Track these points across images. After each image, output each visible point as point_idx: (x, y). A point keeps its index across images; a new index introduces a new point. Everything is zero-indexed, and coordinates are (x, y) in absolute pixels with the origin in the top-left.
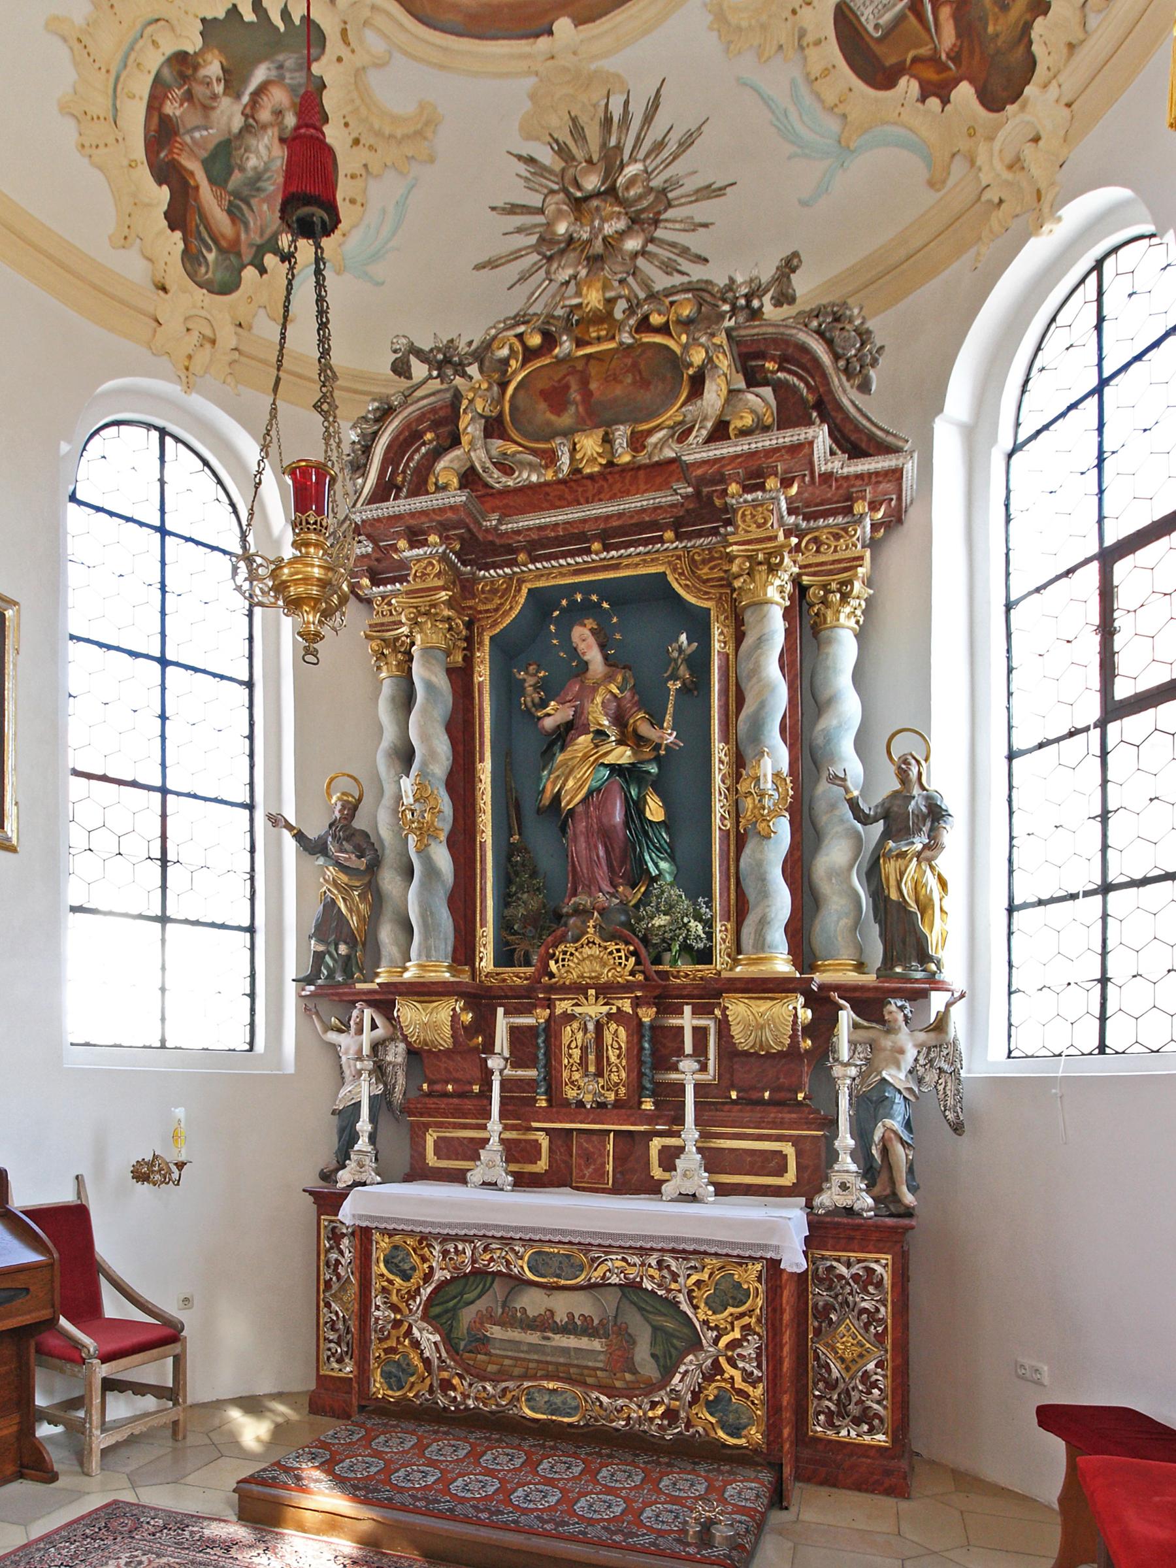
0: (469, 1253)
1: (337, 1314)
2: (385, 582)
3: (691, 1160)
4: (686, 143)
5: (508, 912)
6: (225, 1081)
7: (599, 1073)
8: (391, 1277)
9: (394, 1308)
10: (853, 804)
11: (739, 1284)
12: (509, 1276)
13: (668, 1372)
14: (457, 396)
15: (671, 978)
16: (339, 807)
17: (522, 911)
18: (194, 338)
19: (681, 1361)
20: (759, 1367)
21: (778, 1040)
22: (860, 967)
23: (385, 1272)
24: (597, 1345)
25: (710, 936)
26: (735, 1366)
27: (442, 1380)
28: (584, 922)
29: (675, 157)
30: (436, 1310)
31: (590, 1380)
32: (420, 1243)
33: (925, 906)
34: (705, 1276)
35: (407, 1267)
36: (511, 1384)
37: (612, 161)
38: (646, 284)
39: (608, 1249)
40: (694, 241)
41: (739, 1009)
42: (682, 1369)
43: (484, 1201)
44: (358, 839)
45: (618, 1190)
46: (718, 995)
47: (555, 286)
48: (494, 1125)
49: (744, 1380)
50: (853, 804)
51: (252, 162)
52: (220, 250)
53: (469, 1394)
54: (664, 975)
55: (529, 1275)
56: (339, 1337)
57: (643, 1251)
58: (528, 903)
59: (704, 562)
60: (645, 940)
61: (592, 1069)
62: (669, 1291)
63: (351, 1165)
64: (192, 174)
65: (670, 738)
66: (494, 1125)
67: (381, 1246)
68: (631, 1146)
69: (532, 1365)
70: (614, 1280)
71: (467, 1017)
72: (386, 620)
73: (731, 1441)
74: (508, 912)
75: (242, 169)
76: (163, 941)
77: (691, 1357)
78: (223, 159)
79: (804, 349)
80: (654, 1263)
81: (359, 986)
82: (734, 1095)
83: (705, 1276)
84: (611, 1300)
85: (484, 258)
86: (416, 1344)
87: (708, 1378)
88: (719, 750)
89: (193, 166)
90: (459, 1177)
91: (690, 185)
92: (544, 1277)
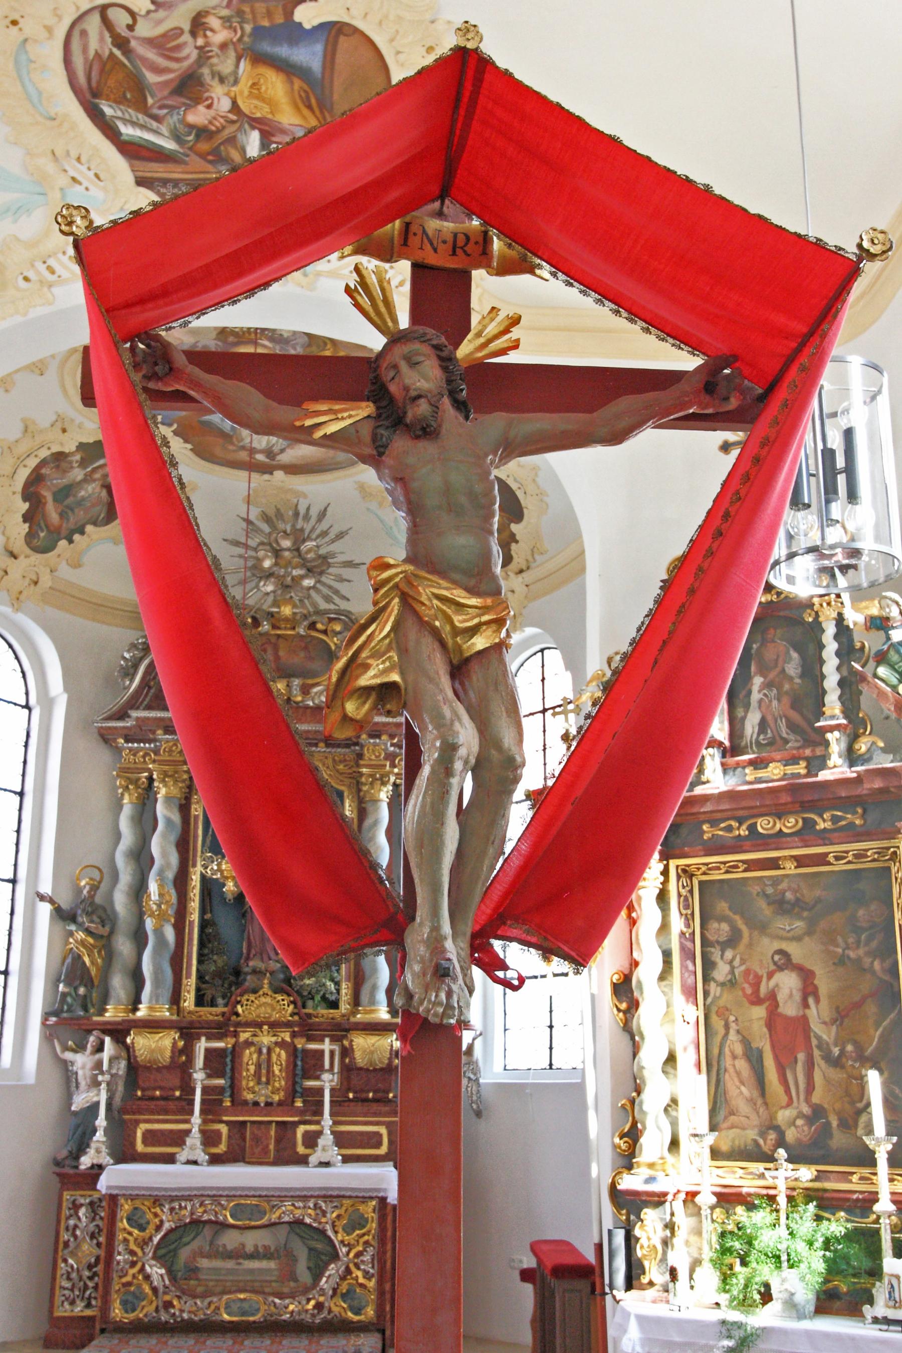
0: (189, 1208)
1: (72, 1267)
2: (133, 742)
3: (327, 1139)
4: (340, 536)
5: (203, 967)
7: (268, 1083)
8: (131, 1229)
9: (132, 1253)
11: (363, 1215)
12: (216, 1223)
13: (317, 1277)
16: (87, 888)
17: (213, 968)
18: (27, 581)
19: (326, 1268)
20: (373, 1267)
21: (381, 1059)
23: (127, 1226)
24: (272, 1264)
25: (338, 991)
26: (359, 1268)
27: (165, 1302)
28: (262, 981)
29: (333, 541)
30: (162, 1252)
31: (267, 1290)
32: (154, 1203)
34: (342, 1211)
35: (143, 1221)
36: (215, 1299)
37: (299, 537)
38: (315, 605)
39: (282, 1198)
41: (361, 1043)
42: (327, 1274)
43: (191, 1172)
44: (100, 912)
45: (276, 1162)
46: (347, 1030)
47: (260, 594)
48: (196, 1119)
49: (364, 1277)
52: (49, 531)
53: (185, 1309)
54: (309, 1016)
55: (231, 1221)
56: (73, 1285)
58: (219, 961)
59: (340, 762)
60: (298, 992)
61: (264, 1079)
62: (320, 1223)
63: (91, 1151)
64: (45, 497)
66: (196, 1119)
67: (126, 1207)
69: (228, 1284)
70: (286, 1219)
71: (181, 1044)
72: (132, 766)
73: (356, 1318)
74: (203, 967)
75: (75, 496)
77: (333, 1266)
78: (64, 493)
80: (311, 1205)
81: (96, 1019)
82: (351, 1095)
83: (342, 1211)
84: (283, 1231)
86: (147, 1277)
87: (343, 1278)
90: (170, 1159)
91: (341, 558)
92: (239, 1220)
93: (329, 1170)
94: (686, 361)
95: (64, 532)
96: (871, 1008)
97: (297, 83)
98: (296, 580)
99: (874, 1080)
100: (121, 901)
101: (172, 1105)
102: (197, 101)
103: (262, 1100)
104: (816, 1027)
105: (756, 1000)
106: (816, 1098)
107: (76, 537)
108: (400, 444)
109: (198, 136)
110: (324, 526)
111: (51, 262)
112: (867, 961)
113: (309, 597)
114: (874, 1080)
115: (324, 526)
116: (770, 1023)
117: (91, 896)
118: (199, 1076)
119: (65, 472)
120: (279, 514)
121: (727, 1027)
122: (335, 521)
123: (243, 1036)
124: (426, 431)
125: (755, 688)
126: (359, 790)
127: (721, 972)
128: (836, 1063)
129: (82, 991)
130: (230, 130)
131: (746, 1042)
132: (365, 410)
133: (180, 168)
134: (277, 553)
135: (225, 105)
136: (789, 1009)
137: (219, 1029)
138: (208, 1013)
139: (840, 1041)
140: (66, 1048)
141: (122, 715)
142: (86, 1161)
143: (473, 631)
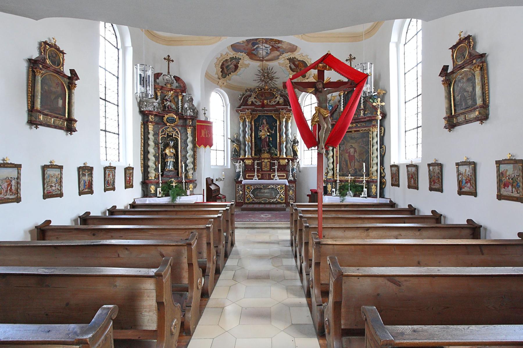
4: (275, 73)
6: (225, 170)
15: (273, 157)
40: (276, 82)
41: (281, 161)
43: (256, 180)
48: (256, 173)
66: (256, 173)
68: (270, 175)
76: (106, 136)
93: (277, 180)
99: (364, 164)
100: (241, 139)
104: (356, 157)
105: (347, 153)
108: (318, 93)
114: (364, 164)
116: (349, 156)
118: (256, 167)
120: (265, 69)
124: (321, 92)
127: (342, 148)
128: (359, 162)
131: (345, 159)
132: (314, 89)
134: (264, 76)
137: (259, 159)
138: (257, 157)
139: (360, 159)
141: (240, 107)
142: (239, 180)
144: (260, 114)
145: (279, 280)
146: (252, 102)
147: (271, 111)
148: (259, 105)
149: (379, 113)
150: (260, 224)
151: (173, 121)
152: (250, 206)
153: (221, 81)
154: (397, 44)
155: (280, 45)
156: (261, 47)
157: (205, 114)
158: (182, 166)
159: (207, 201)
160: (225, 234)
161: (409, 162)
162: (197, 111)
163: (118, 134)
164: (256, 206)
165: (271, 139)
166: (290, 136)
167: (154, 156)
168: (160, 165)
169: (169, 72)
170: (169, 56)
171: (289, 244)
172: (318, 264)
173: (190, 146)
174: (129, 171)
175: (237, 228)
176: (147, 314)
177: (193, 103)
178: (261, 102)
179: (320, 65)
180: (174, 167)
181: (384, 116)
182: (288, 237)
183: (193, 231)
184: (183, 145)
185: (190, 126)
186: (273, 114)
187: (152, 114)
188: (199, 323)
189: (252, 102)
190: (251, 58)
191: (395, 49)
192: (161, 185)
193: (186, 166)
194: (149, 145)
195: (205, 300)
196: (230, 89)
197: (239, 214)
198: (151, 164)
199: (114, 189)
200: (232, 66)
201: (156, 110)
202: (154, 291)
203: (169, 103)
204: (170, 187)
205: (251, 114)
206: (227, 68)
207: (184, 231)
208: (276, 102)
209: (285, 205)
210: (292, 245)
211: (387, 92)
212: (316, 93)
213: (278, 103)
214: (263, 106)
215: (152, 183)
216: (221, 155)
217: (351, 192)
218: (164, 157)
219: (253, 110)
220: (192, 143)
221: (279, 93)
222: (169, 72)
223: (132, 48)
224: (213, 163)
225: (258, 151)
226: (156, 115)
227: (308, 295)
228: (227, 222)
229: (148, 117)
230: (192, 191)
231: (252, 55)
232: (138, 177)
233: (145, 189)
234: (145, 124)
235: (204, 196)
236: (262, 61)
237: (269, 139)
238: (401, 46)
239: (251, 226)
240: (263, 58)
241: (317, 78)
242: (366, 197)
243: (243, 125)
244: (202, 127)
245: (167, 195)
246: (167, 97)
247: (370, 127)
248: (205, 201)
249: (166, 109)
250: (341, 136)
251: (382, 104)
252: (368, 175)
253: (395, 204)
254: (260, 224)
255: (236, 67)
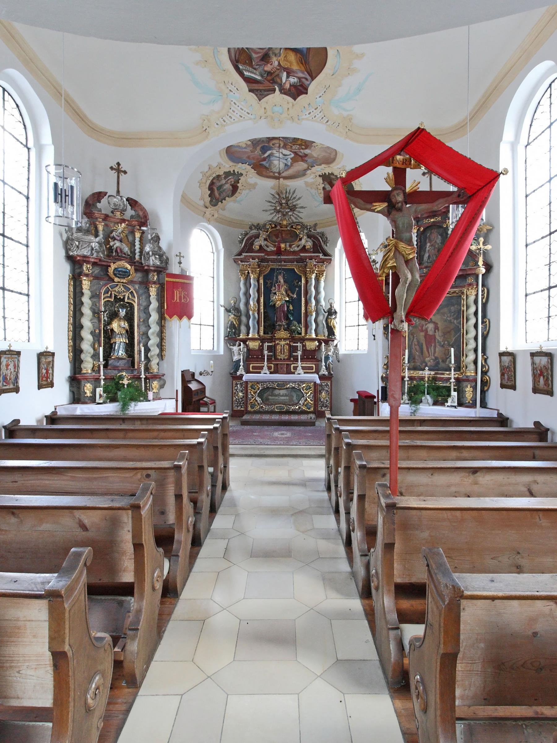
4: (299, 199)
6: (215, 357)
10: (324, 310)
14: (259, 234)
15: (295, 338)
22: (324, 336)
29: (297, 200)
33: (334, 327)
38: (292, 220)
40: (300, 214)
43: (265, 375)
48: (266, 363)
50: (324, 310)
51: (225, 187)
53: (266, 408)
57: (295, 382)
65: (295, 296)
66: (266, 363)
68: (288, 366)
76: (4, 298)
79: (317, 238)
85: (264, 209)
86: (256, 401)
87: (305, 401)
88: (303, 299)
89: (215, 188)
90: (260, 373)
93: (300, 375)
94: (452, 188)
95: (220, 200)
96: (453, 333)
97: (299, 55)
98: (287, 213)
99: (452, 350)
100: (242, 307)
101: (259, 359)
102: (268, 62)
103: (282, 358)
104: (437, 337)
105: (422, 331)
106: (436, 355)
107: (223, 201)
108: (394, 213)
109: (267, 75)
110: (294, 196)
111: (224, 118)
112: (453, 320)
113: (291, 218)
114: (452, 350)
115: (294, 196)
117: (234, 306)
118: (266, 352)
119: (220, 181)
120: (282, 192)
121: (414, 337)
122: (298, 194)
123: (277, 342)
124: (400, 210)
125: (428, 247)
126: (306, 275)
128: (443, 346)
129: (233, 331)
130: (278, 72)
131: (418, 342)
132: (386, 204)
133: (261, 85)
134: (281, 204)
135: (276, 63)
136: (431, 333)
137: (271, 340)
138: (268, 336)
139: (444, 341)
140: (230, 345)
142: (238, 373)
143: (410, 254)
144: (275, 266)
145: (308, 560)
146: (261, 246)
147: (292, 261)
148: (272, 251)
149: (481, 263)
150: (272, 449)
151: (124, 274)
152: (257, 417)
153: (209, 211)
154: (514, 146)
155: (307, 151)
156: (277, 155)
157: (180, 263)
158: (140, 351)
159: (184, 410)
160: (211, 470)
161: (535, 348)
162: (167, 259)
163: (28, 295)
164: (266, 417)
165: (291, 308)
166: (323, 303)
167: (91, 333)
168: (101, 349)
169: (118, 192)
170: (118, 164)
171: (322, 486)
172: (362, 498)
173: (154, 316)
174: (45, 359)
175: (233, 455)
176: (31, 672)
177: (161, 245)
178: (275, 246)
179: (399, 157)
180: (126, 351)
181: (489, 267)
182: (322, 474)
183: (149, 472)
184: (143, 315)
185: (154, 283)
186: (295, 267)
187: (88, 262)
188: (158, 655)
189: (261, 246)
190: (260, 174)
191: (509, 154)
192: (102, 382)
193: (147, 350)
194: (82, 314)
195: (171, 603)
196: (224, 225)
197: (237, 431)
198: (86, 346)
199: (16, 390)
200: (228, 187)
201: (95, 255)
202: (46, 624)
203: (118, 244)
204: (119, 386)
205: (259, 266)
206: (221, 189)
207: (135, 472)
208: (300, 247)
209: (313, 416)
210: (329, 489)
211: (493, 227)
212: (392, 210)
213: (304, 249)
214: (279, 252)
215: (87, 380)
216: (208, 332)
217: (428, 397)
218: (109, 335)
219: (262, 260)
220: (158, 312)
221: (305, 231)
222: (118, 192)
223: (53, 147)
224: (195, 345)
225: (270, 327)
226: (94, 264)
227: (366, 593)
228: (218, 447)
229: (81, 266)
230: (157, 393)
231: (261, 168)
232: (62, 369)
233: (75, 390)
234: (76, 279)
235: (177, 401)
236: (278, 178)
237: (288, 307)
238: (521, 148)
239: (257, 452)
240: (279, 173)
241: (393, 182)
242: (455, 407)
243: (245, 284)
244: (175, 285)
245: (113, 400)
246: (114, 234)
247: (464, 287)
248: (180, 410)
249: (113, 254)
250: (438, 299)
251: (486, 247)
252: (458, 368)
253: (508, 419)
254: (272, 449)
255: (235, 188)
